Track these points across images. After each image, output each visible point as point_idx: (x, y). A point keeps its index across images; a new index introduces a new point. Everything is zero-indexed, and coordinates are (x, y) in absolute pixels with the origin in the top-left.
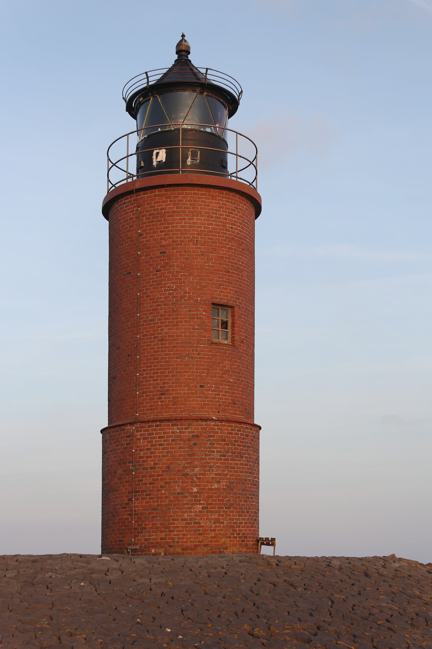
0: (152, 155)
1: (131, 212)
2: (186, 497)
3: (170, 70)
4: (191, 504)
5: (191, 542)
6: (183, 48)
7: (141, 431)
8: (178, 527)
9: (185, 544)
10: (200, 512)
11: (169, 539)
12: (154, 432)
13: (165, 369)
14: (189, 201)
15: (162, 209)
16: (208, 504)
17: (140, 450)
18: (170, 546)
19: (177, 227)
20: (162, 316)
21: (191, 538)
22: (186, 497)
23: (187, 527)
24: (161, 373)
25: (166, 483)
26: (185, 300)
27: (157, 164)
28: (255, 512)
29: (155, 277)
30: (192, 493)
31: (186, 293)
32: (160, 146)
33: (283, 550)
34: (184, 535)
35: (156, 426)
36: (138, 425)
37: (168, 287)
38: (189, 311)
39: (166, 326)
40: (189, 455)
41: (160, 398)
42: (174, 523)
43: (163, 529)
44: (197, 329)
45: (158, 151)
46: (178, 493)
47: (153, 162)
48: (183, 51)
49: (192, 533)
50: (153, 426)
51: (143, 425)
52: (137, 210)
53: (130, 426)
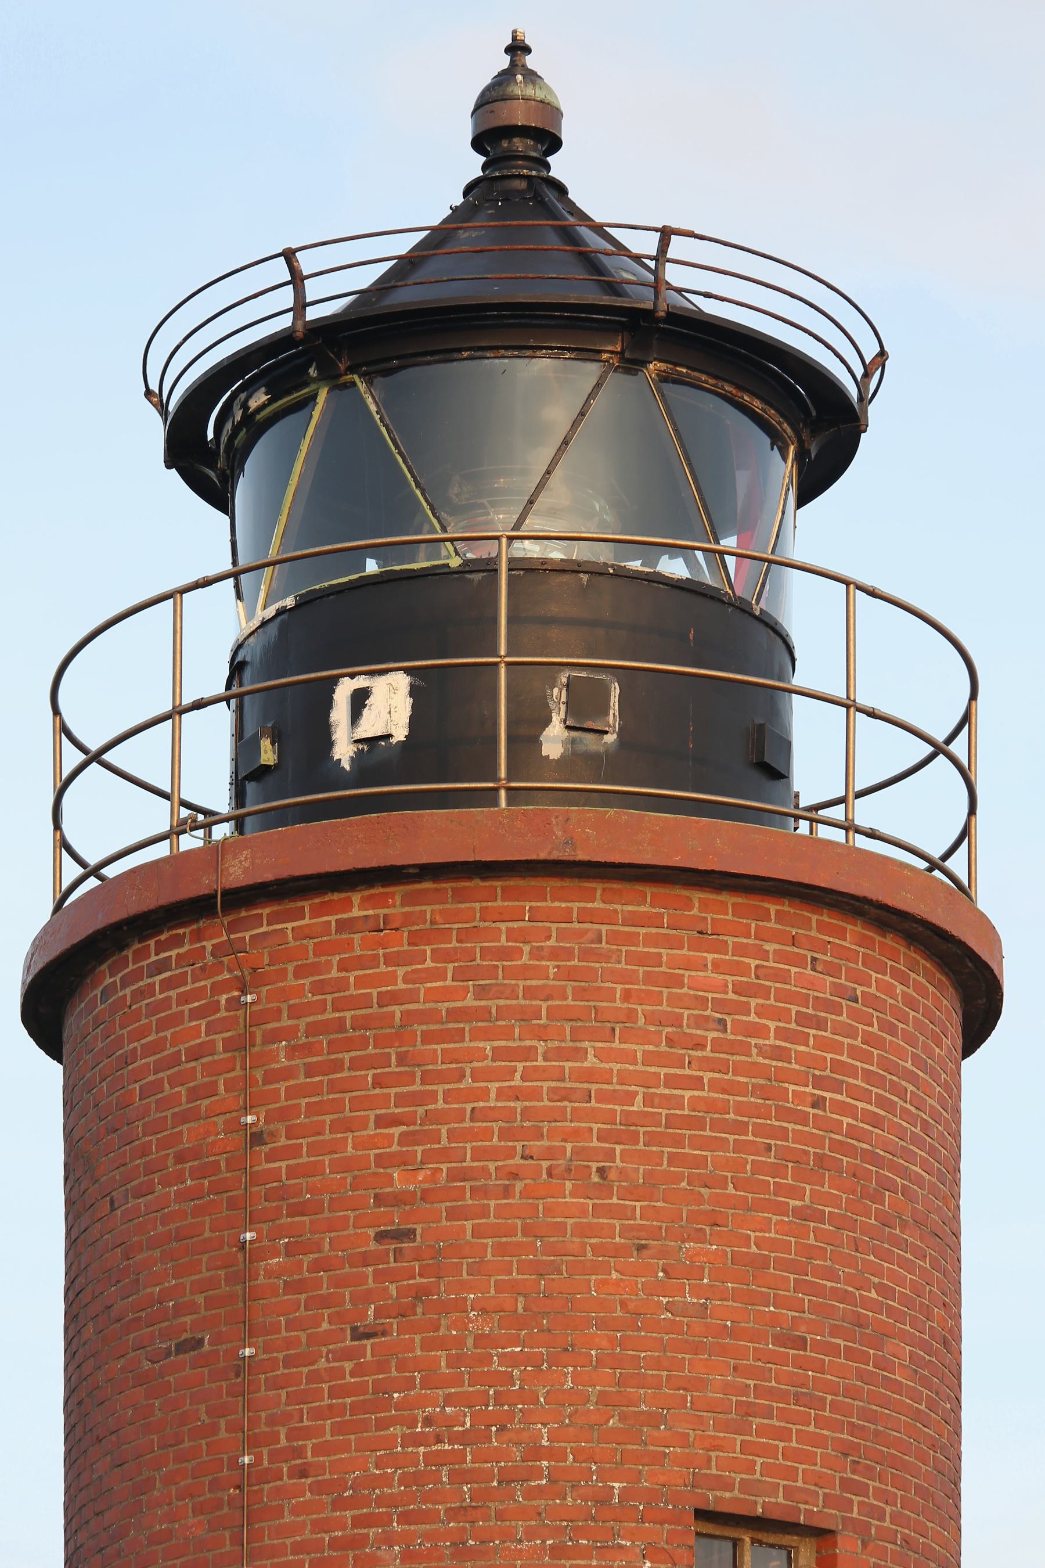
0: (328, 704)
1: (195, 1014)
3: (438, 238)
14: (555, 954)
27: (359, 753)
29: (348, 1366)
31: (535, 1452)
32: (374, 653)
37: (428, 1421)
45: (361, 682)
47: (330, 744)
48: (515, 138)
52: (234, 1004)
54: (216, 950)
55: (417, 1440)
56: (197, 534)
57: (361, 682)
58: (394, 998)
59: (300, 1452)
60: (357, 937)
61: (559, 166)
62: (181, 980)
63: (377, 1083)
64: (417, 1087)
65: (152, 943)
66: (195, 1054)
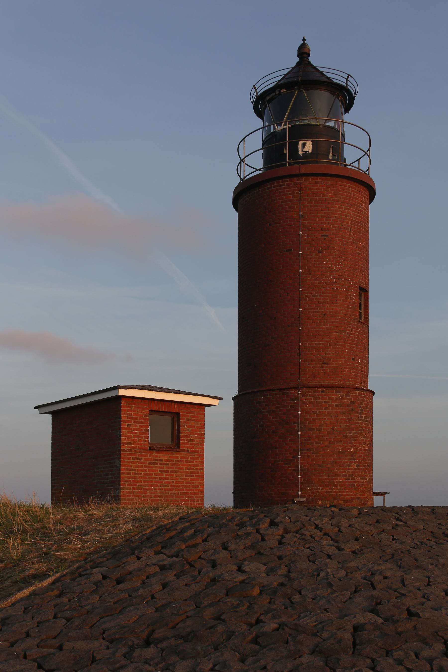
0: (298, 144)
1: (290, 194)
2: (346, 456)
3: (293, 68)
4: (350, 463)
5: (349, 495)
6: (306, 51)
7: (307, 395)
8: (340, 482)
9: (345, 497)
10: (355, 469)
11: (334, 492)
12: (320, 397)
13: (327, 341)
14: (346, 192)
15: (324, 196)
16: (360, 463)
17: (306, 413)
18: (334, 499)
19: (337, 214)
20: (323, 293)
21: (350, 491)
22: (346, 456)
23: (347, 482)
24: (323, 344)
25: (330, 443)
26: (343, 281)
27: (303, 153)
28: (370, 470)
29: (317, 257)
30: (350, 452)
31: (343, 275)
32: (306, 137)
33: (391, 502)
34: (345, 489)
35: (322, 392)
36: (304, 390)
37: (329, 267)
38: (346, 291)
39: (327, 303)
40: (348, 419)
41: (322, 367)
42: (338, 479)
43: (328, 484)
44: (350, 308)
45: (304, 142)
46: (340, 452)
47: (298, 151)
48: (303, 52)
49: (350, 487)
50: (319, 392)
51: (309, 390)
52: (298, 193)
53: (295, 390)
54: (295, 184)
55: (328, 271)
56: (259, 123)
57: (304, 142)
58: (324, 196)
59: (310, 270)
60: (319, 185)
61: (310, 59)
62: (287, 188)
63: (322, 210)
64: (328, 211)
65: (281, 181)
66: (290, 201)
